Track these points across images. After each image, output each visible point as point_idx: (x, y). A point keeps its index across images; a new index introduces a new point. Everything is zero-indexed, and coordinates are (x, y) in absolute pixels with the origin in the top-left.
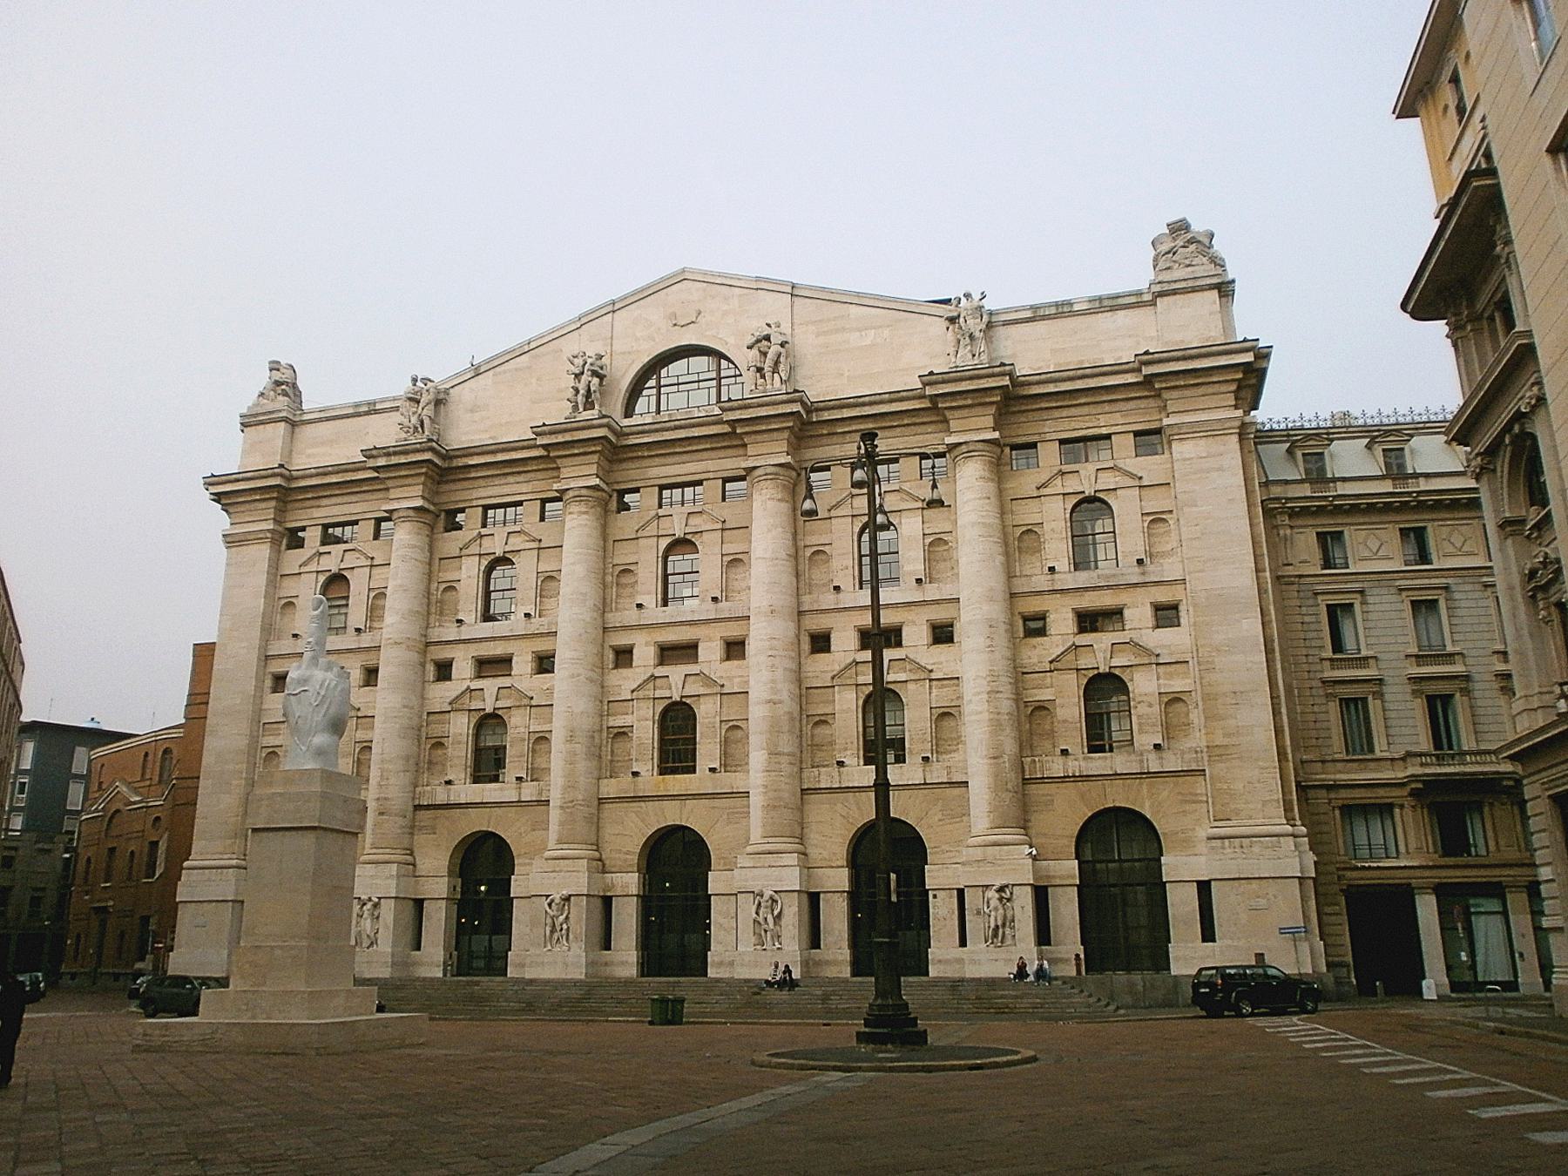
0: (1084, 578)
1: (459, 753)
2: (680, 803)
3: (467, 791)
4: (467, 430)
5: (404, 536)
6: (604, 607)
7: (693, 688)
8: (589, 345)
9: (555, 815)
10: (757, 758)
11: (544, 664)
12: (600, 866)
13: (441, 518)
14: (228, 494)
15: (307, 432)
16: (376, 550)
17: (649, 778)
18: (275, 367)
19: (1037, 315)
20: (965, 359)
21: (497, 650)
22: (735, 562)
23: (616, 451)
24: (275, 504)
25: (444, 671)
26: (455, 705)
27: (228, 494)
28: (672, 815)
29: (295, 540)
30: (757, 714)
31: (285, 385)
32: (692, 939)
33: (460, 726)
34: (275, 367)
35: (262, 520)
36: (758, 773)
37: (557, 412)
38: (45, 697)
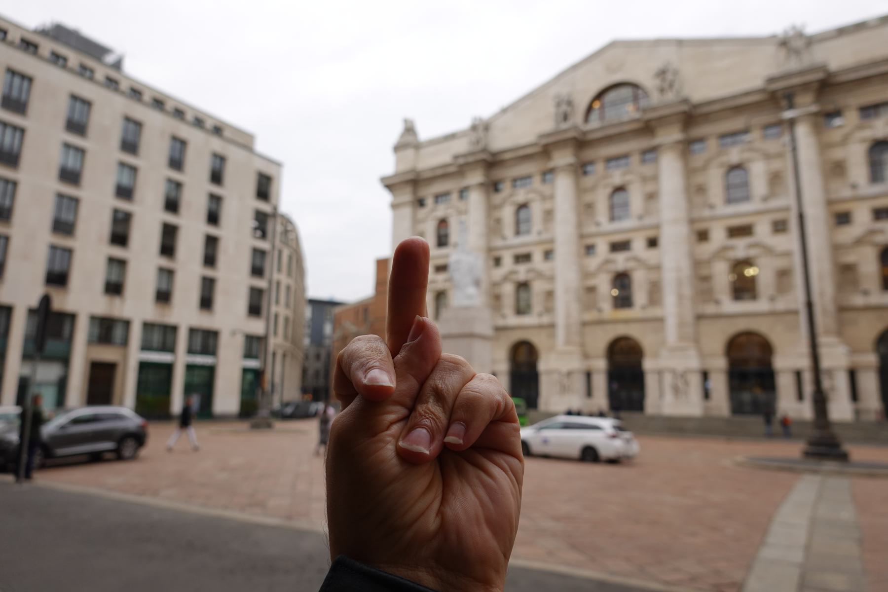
0: (877, 189)
1: (508, 301)
2: (629, 324)
3: (513, 320)
4: (500, 142)
5: (476, 198)
6: (580, 225)
7: (630, 265)
8: (563, 90)
9: (561, 333)
10: (670, 299)
11: (548, 255)
12: (586, 356)
13: (493, 186)
14: (390, 185)
15: (424, 152)
16: (461, 205)
17: (607, 309)
18: (406, 121)
19: (842, 32)
20: (793, 65)
21: (523, 251)
22: (651, 197)
23: (581, 143)
24: (411, 186)
25: (498, 261)
26: (506, 279)
27: (390, 185)
28: (621, 330)
29: (421, 203)
30: (669, 278)
31: (409, 129)
32: (635, 394)
33: (508, 289)
34: (406, 121)
35: (407, 196)
36: (671, 307)
37: (548, 126)
38: (317, 287)
